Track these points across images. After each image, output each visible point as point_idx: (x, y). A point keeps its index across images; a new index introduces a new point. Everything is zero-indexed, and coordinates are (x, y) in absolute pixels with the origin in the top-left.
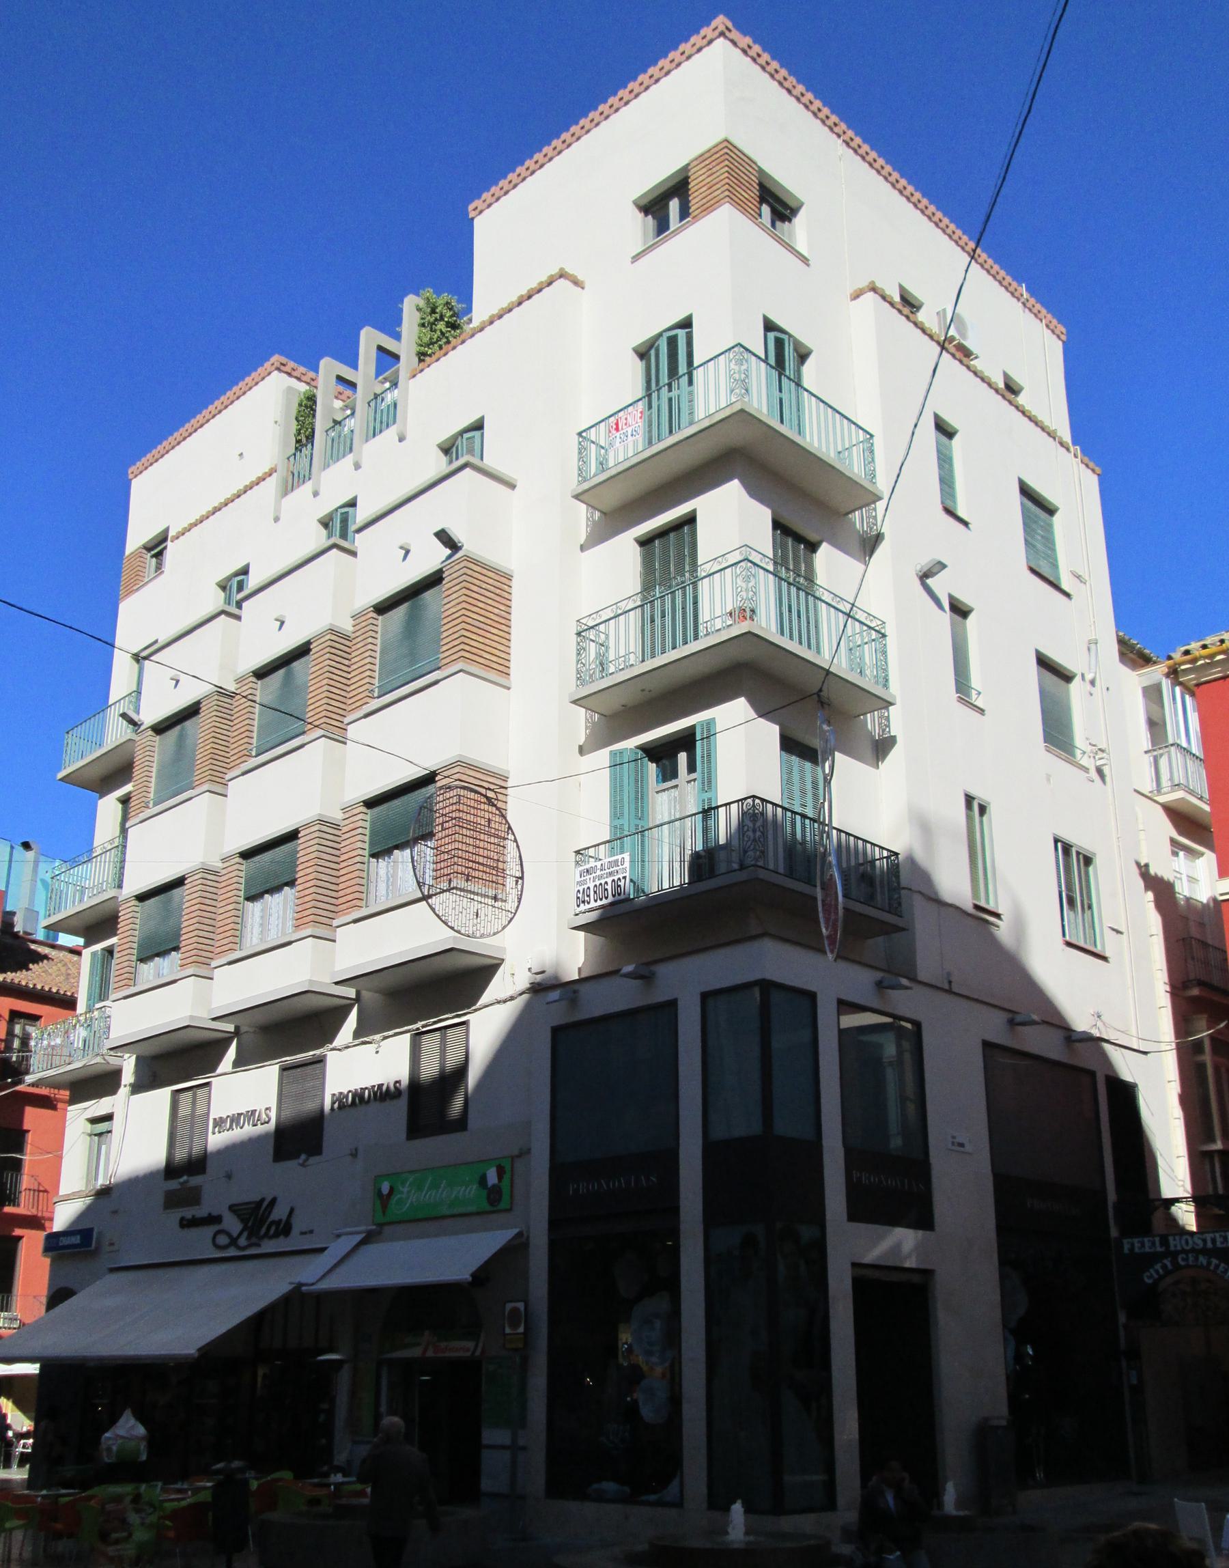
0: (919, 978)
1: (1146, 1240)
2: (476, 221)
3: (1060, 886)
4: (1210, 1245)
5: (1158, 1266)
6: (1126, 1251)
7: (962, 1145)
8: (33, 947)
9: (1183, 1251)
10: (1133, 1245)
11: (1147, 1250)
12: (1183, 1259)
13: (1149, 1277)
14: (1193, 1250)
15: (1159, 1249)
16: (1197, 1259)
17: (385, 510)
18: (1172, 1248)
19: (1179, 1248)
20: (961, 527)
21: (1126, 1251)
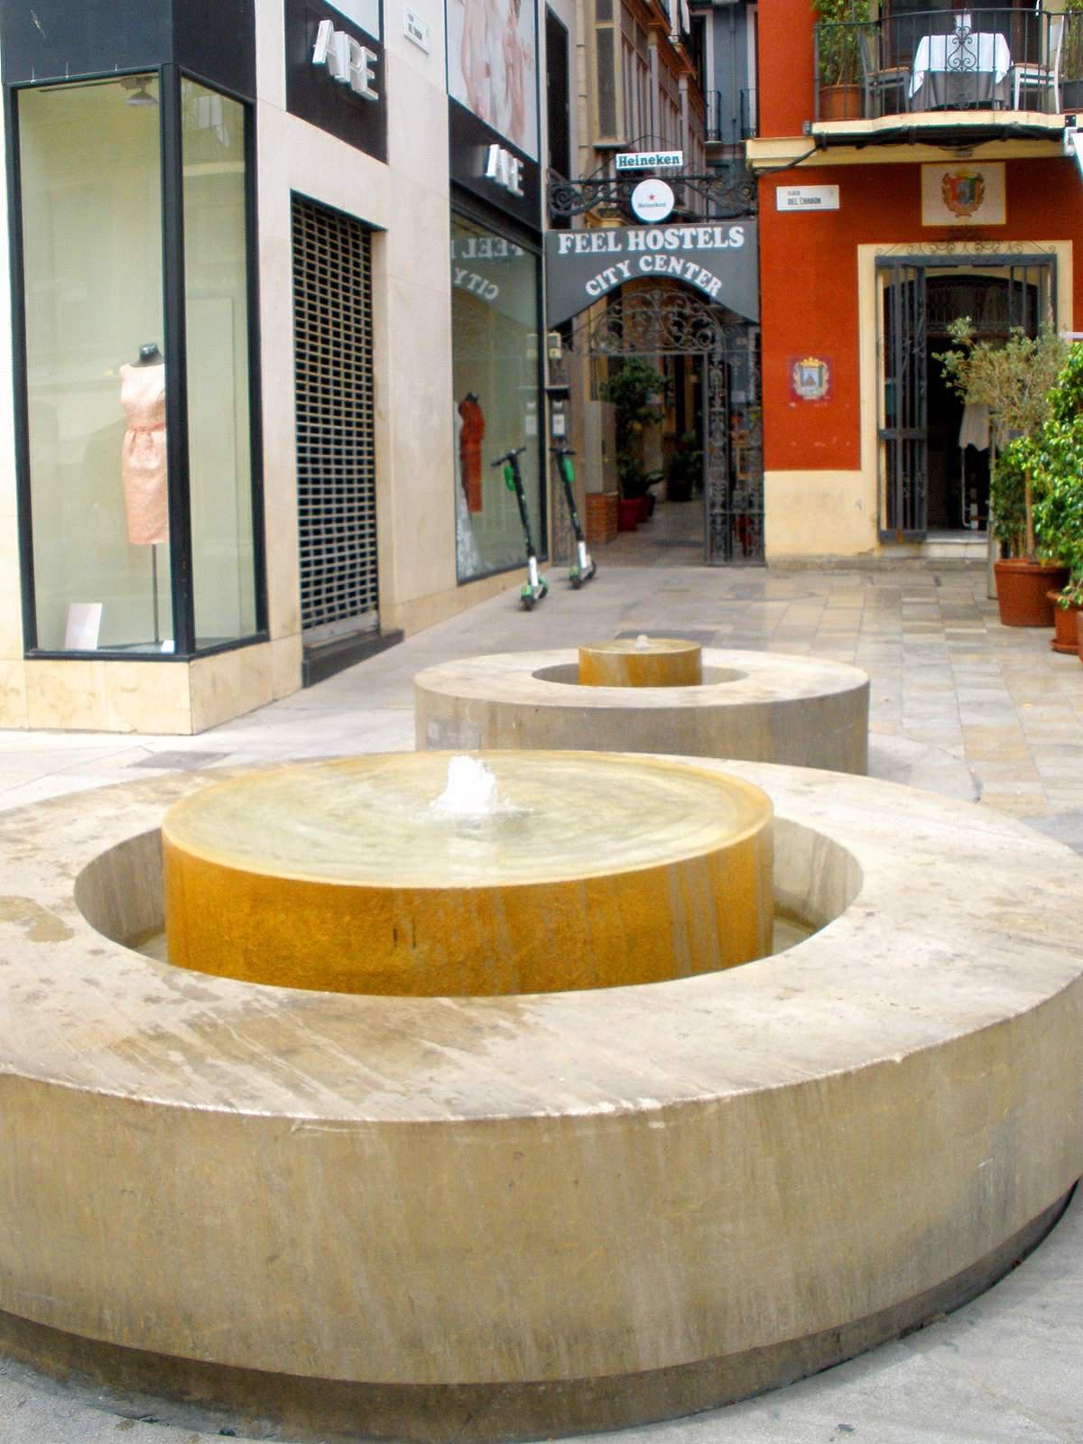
0: (855, 579)
1: (594, 237)
2: (519, 457)
3: (78, 87)
4: (688, 245)
5: (609, 273)
6: (563, 251)
7: (419, 35)
8: (688, 30)
9: (648, 252)
10: (574, 242)
11: (595, 249)
12: (647, 264)
13: (594, 287)
14: (663, 251)
15: (612, 248)
16: (667, 263)
17: (874, 296)
18: (632, 248)
19: (642, 248)
20: (421, 55)
21: (563, 251)
